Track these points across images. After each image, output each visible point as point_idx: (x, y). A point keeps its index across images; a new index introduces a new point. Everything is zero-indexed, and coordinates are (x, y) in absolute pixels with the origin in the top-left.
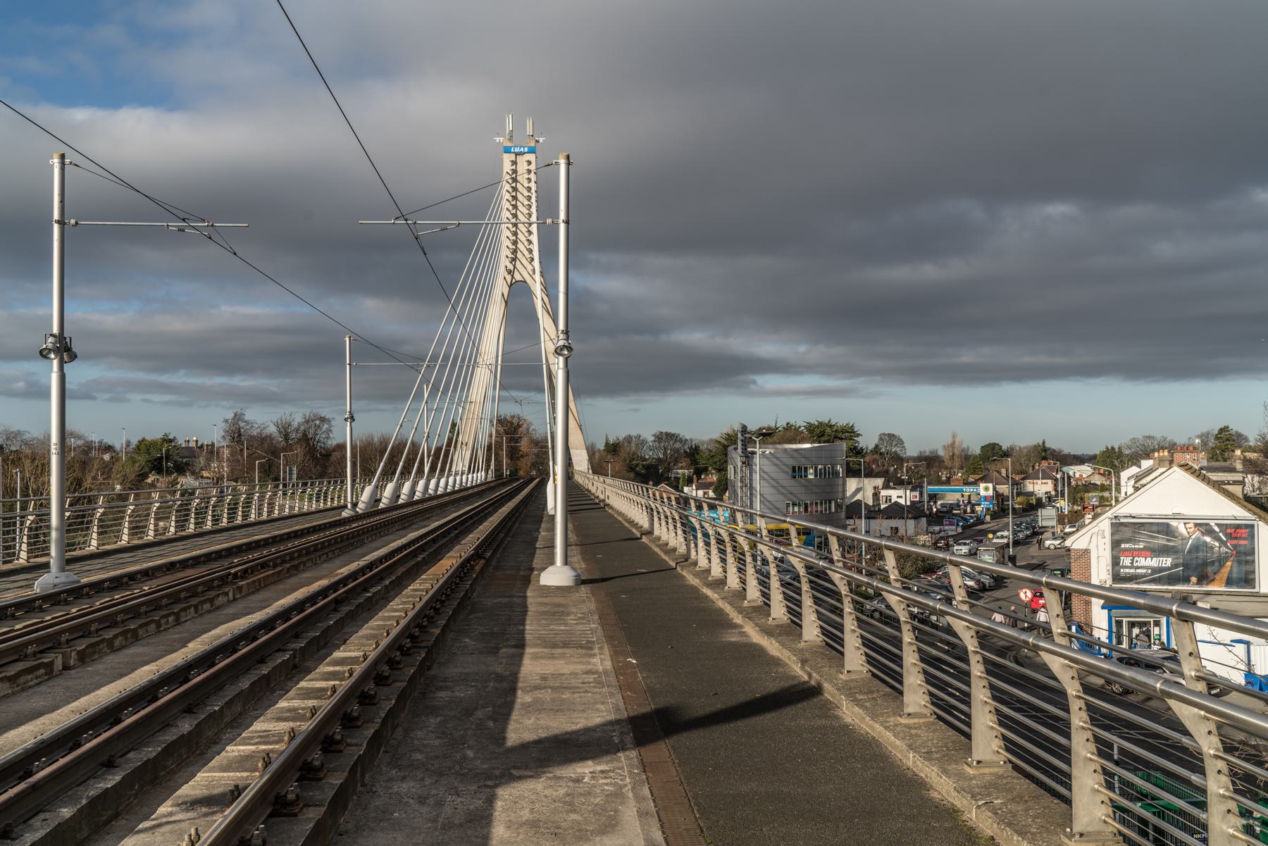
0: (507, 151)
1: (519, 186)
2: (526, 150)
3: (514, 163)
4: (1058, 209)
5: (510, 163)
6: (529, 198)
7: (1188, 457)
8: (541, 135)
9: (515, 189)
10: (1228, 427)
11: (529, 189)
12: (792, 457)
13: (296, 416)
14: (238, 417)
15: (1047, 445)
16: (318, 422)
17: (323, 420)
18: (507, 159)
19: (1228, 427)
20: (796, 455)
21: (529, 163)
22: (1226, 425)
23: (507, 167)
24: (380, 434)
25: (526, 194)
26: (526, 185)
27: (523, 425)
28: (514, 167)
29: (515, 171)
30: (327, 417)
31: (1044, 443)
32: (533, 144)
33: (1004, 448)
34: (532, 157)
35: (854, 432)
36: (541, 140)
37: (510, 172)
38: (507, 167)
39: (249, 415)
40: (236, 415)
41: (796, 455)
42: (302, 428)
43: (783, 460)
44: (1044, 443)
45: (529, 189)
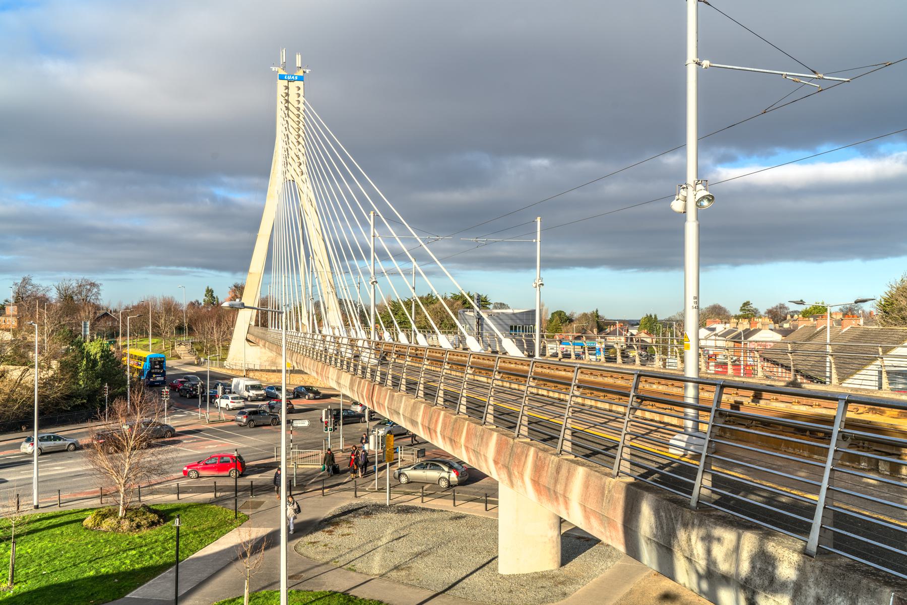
0: (282, 77)
1: (290, 106)
2: (296, 78)
3: (287, 88)
4: (541, 162)
5: (284, 88)
6: (298, 116)
7: (854, 322)
8: (308, 67)
9: (287, 108)
10: (749, 302)
11: (298, 109)
12: (512, 319)
13: (72, 280)
14: (26, 281)
15: (600, 314)
17: (93, 285)
18: (281, 84)
19: (749, 302)
20: (514, 317)
21: (299, 89)
22: (748, 300)
23: (281, 90)
24: (161, 298)
25: (296, 112)
26: (296, 106)
27: (461, 293)
28: (286, 91)
29: (287, 94)
30: (96, 283)
31: (597, 311)
32: (302, 74)
33: (567, 314)
34: (300, 84)
35: (487, 302)
36: (308, 71)
37: (284, 95)
38: (281, 90)
39: (35, 281)
40: (24, 279)
41: (514, 317)
43: (506, 321)
44: (597, 311)
45: (298, 109)
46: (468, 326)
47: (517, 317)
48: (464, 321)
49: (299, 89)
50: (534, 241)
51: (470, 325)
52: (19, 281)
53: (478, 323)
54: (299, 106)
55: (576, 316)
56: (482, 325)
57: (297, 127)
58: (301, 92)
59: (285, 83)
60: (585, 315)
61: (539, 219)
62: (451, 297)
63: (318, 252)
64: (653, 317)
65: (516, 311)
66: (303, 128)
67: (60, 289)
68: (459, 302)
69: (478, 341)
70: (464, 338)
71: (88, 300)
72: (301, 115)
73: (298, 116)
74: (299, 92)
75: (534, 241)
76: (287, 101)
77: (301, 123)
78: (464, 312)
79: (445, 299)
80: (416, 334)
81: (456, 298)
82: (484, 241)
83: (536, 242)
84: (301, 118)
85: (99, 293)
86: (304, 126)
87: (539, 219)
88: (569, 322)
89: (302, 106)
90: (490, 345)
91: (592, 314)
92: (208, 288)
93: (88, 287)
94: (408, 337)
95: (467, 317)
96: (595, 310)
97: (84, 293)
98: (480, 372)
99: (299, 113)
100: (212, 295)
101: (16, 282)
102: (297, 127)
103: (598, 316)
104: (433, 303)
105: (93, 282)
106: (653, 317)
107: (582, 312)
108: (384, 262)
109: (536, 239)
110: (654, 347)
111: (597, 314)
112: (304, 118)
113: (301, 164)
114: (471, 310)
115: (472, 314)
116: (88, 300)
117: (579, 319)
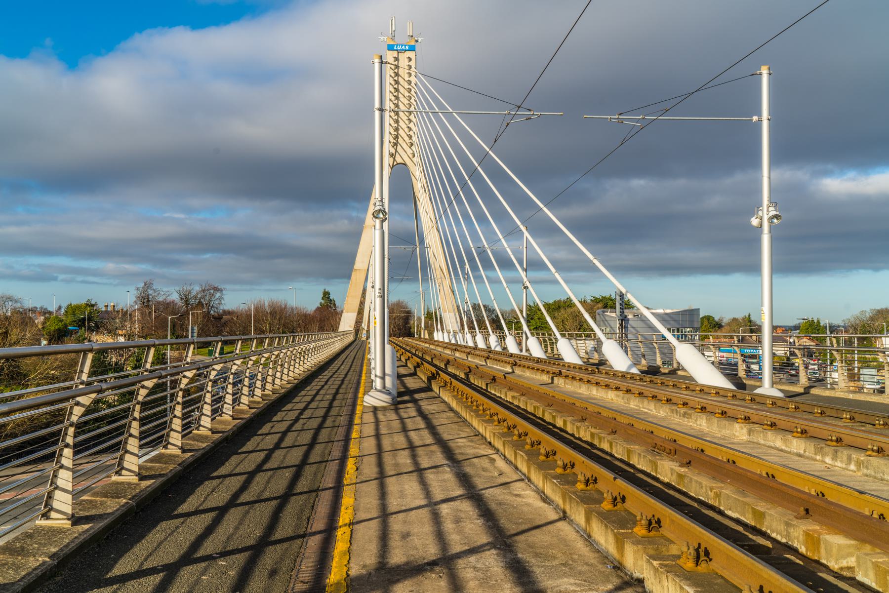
1: (400, 80)
2: (407, 48)
3: (397, 59)
6: (409, 91)
9: (397, 82)
11: (409, 82)
15: (752, 318)
16: (212, 291)
17: (216, 289)
20: (668, 319)
21: (410, 59)
25: (407, 86)
26: (407, 79)
30: (219, 287)
31: (749, 315)
33: (716, 319)
34: (411, 54)
35: (630, 305)
36: (420, 40)
41: (668, 319)
42: (199, 296)
44: (749, 315)
45: (409, 82)
46: (608, 330)
47: (670, 317)
48: (603, 323)
49: (410, 59)
50: (755, 118)
51: (611, 327)
52: (141, 285)
53: (621, 325)
54: (410, 79)
55: (725, 321)
56: (626, 328)
57: (408, 102)
58: (413, 63)
59: (395, 54)
60: (735, 320)
61: (765, 71)
62: (591, 300)
63: (433, 245)
64: (816, 321)
65: (668, 311)
66: (415, 103)
67: (182, 294)
68: (600, 305)
69: (626, 352)
70: (599, 343)
71: (211, 305)
72: (413, 90)
73: (409, 91)
74: (410, 63)
75: (755, 118)
76: (397, 74)
77: (413, 98)
78: (604, 312)
79: (583, 303)
80: (527, 338)
81: (596, 301)
82: (638, 121)
83: (760, 121)
84: (413, 92)
85: (222, 298)
86: (416, 101)
87: (765, 71)
88: (719, 328)
89: (413, 79)
90: (644, 356)
91: (744, 319)
92: (325, 290)
93: (212, 291)
94: (543, 343)
95: (607, 318)
96: (747, 315)
97: (207, 298)
98: (654, 524)
99: (410, 87)
100: (329, 298)
101: (138, 286)
102: (408, 102)
103: (750, 321)
104: (571, 307)
105: (216, 286)
106: (816, 321)
107: (732, 317)
108: (563, 298)
109: (760, 114)
110: (655, 344)
111: (749, 318)
112: (416, 93)
113: (412, 144)
114: (612, 310)
115: (614, 315)
116: (211, 305)
117: (729, 324)
